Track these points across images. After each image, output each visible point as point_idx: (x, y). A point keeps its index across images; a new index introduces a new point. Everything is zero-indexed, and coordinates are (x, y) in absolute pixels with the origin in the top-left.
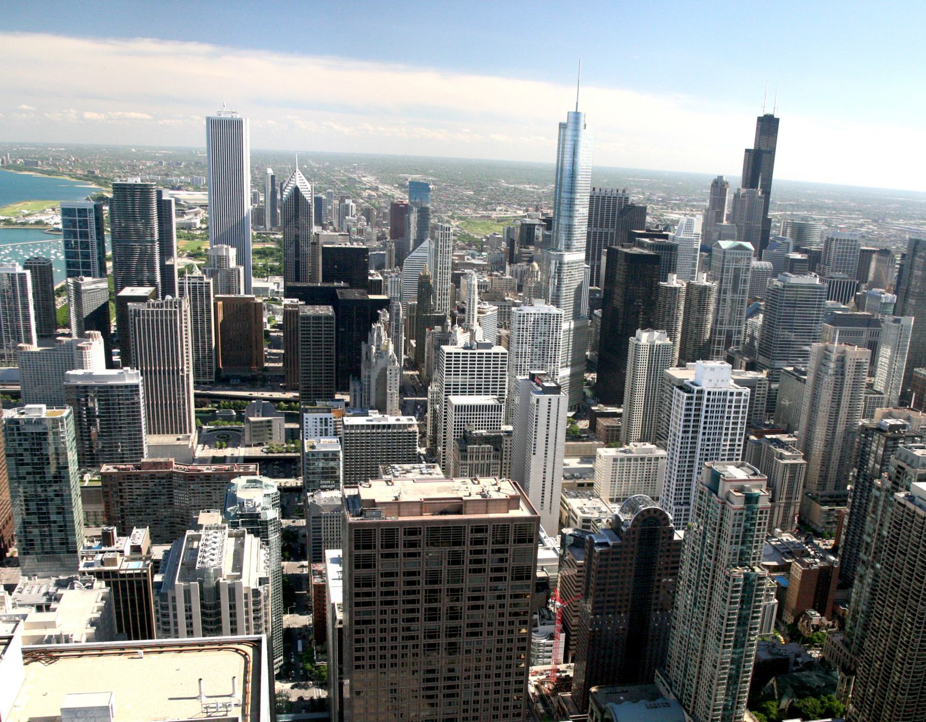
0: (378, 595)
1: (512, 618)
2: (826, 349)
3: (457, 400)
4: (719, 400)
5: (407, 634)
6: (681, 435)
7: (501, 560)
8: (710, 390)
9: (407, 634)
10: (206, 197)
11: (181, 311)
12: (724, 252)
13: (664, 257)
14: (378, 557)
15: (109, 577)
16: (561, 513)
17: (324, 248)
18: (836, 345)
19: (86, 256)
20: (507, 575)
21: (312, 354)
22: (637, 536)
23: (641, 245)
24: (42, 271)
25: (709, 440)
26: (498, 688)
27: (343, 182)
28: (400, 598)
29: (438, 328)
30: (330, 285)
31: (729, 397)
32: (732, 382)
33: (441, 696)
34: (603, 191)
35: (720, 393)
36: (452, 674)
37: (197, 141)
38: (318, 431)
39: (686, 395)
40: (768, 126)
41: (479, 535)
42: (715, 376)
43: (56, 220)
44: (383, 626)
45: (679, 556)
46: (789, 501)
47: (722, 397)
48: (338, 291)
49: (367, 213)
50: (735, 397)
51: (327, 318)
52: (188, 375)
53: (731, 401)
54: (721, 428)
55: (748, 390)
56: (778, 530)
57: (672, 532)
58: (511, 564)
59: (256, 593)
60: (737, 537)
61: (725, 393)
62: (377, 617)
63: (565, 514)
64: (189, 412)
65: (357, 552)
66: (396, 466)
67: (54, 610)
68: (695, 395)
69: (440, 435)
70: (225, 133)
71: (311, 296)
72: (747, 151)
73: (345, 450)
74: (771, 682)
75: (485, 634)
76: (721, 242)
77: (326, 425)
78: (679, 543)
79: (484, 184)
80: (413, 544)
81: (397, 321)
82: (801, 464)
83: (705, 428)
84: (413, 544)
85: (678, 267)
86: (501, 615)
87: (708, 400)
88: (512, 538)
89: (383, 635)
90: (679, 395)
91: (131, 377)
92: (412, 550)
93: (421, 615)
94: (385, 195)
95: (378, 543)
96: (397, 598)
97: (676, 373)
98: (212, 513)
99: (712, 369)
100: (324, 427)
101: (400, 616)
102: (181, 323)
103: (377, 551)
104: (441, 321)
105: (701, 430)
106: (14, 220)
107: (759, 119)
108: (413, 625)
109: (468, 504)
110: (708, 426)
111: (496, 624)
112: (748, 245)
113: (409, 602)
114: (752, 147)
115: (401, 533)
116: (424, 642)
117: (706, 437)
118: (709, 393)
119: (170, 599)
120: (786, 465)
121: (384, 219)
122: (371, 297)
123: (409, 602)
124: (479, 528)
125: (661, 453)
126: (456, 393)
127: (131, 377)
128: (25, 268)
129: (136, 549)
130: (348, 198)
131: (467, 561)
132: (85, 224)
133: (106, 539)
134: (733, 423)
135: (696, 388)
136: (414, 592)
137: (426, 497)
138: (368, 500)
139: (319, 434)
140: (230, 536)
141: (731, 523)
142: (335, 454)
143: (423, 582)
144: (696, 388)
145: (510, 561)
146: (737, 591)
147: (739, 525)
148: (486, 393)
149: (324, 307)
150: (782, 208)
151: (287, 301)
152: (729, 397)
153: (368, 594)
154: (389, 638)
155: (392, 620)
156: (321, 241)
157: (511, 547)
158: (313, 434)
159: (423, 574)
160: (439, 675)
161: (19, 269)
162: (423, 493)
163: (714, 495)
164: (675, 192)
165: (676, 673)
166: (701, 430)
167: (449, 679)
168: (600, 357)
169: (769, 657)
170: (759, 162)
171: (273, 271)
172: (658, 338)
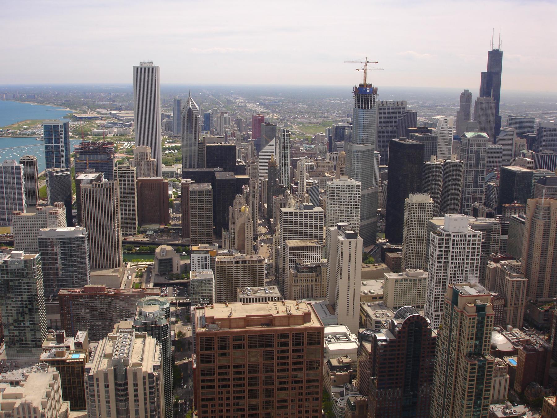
2: (537, 202)
4: (461, 241)
5: (236, 407)
6: (436, 264)
7: (299, 357)
8: (454, 234)
9: (236, 407)
10: (133, 115)
12: (469, 140)
13: (429, 144)
15: (59, 364)
16: (361, 318)
17: (207, 146)
18: (543, 200)
19: (58, 154)
20: (304, 366)
21: (197, 215)
23: (412, 138)
24: (30, 165)
25: (455, 267)
27: (224, 102)
28: (231, 383)
29: (281, 196)
30: (212, 170)
32: (469, 227)
34: (384, 103)
35: (461, 236)
37: (126, 79)
38: (201, 265)
39: (438, 237)
40: (495, 57)
41: (283, 340)
42: (456, 223)
43: (41, 131)
44: (221, 402)
45: (435, 348)
46: (516, 306)
48: (216, 173)
49: (238, 122)
50: (471, 238)
52: (118, 230)
53: (469, 241)
55: (481, 233)
56: (510, 326)
57: (430, 331)
58: (305, 359)
59: (151, 375)
61: (465, 236)
62: (217, 396)
63: (364, 318)
64: (119, 253)
66: (249, 288)
67: (22, 386)
68: (444, 237)
70: (146, 75)
71: (199, 178)
72: (482, 73)
73: (217, 279)
76: (466, 134)
77: (206, 261)
78: (434, 338)
81: (254, 192)
82: (524, 281)
83: (452, 259)
85: (438, 149)
86: (301, 394)
88: (305, 342)
89: (221, 408)
91: (79, 231)
93: (246, 394)
94: (251, 110)
95: (216, 347)
96: (233, 383)
97: (436, 221)
98: (128, 321)
99: (456, 220)
100: (204, 263)
101: (232, 395)
102: (114, 197)
103: (216, 352)
104: (283, 191)
105: (450, 261)
106: (18, 132)
108: (241, 402)
109: (276, 319)
110: (454, 258)
112: (484, 134)
113: (238, 385)
114: (486, 71)
115: (276, 337)
116: (248, 412)
118: (454, 236)
119: (95, 380)
120: (513, 281)
121: (249, 126)
122: (237, 177)
123: (238, 385)
124: (284, 335)
125: (426, 274)
126: (290, 238)
127: (79, 231)
128: (21, 163)
129: (78, 345)
130: (226, 113)
131: (276, 358)
132: (57, 135)
133: (60, 339)
135: (445, 233)
136: (241, 379)
137: (248, 314)
138: (210, 318)
139: (201, 267)
140: (137, 337)
141: (468, 325)
142: (210, 280)
143: (246, 372)
145: (305, 357)
147: (473, 327)
148: (311, 238)
149: (206, 185)
151: (183, 181)
152: (467, 238)
153: (211, 381)
154: (224, 410)
155: (227, 398)
156: (206, 142)
157: (305, 347)
158: (197, 267)
159: (246, 367)
161: (17, 164)
162: (247, 312)
163: (455, 306)
164: (436, 103)
166: (450, 261)
168: (388, 211)
169: (503, 416)
170: (491, 80)
171: (177, 161)
172: (424, 199)
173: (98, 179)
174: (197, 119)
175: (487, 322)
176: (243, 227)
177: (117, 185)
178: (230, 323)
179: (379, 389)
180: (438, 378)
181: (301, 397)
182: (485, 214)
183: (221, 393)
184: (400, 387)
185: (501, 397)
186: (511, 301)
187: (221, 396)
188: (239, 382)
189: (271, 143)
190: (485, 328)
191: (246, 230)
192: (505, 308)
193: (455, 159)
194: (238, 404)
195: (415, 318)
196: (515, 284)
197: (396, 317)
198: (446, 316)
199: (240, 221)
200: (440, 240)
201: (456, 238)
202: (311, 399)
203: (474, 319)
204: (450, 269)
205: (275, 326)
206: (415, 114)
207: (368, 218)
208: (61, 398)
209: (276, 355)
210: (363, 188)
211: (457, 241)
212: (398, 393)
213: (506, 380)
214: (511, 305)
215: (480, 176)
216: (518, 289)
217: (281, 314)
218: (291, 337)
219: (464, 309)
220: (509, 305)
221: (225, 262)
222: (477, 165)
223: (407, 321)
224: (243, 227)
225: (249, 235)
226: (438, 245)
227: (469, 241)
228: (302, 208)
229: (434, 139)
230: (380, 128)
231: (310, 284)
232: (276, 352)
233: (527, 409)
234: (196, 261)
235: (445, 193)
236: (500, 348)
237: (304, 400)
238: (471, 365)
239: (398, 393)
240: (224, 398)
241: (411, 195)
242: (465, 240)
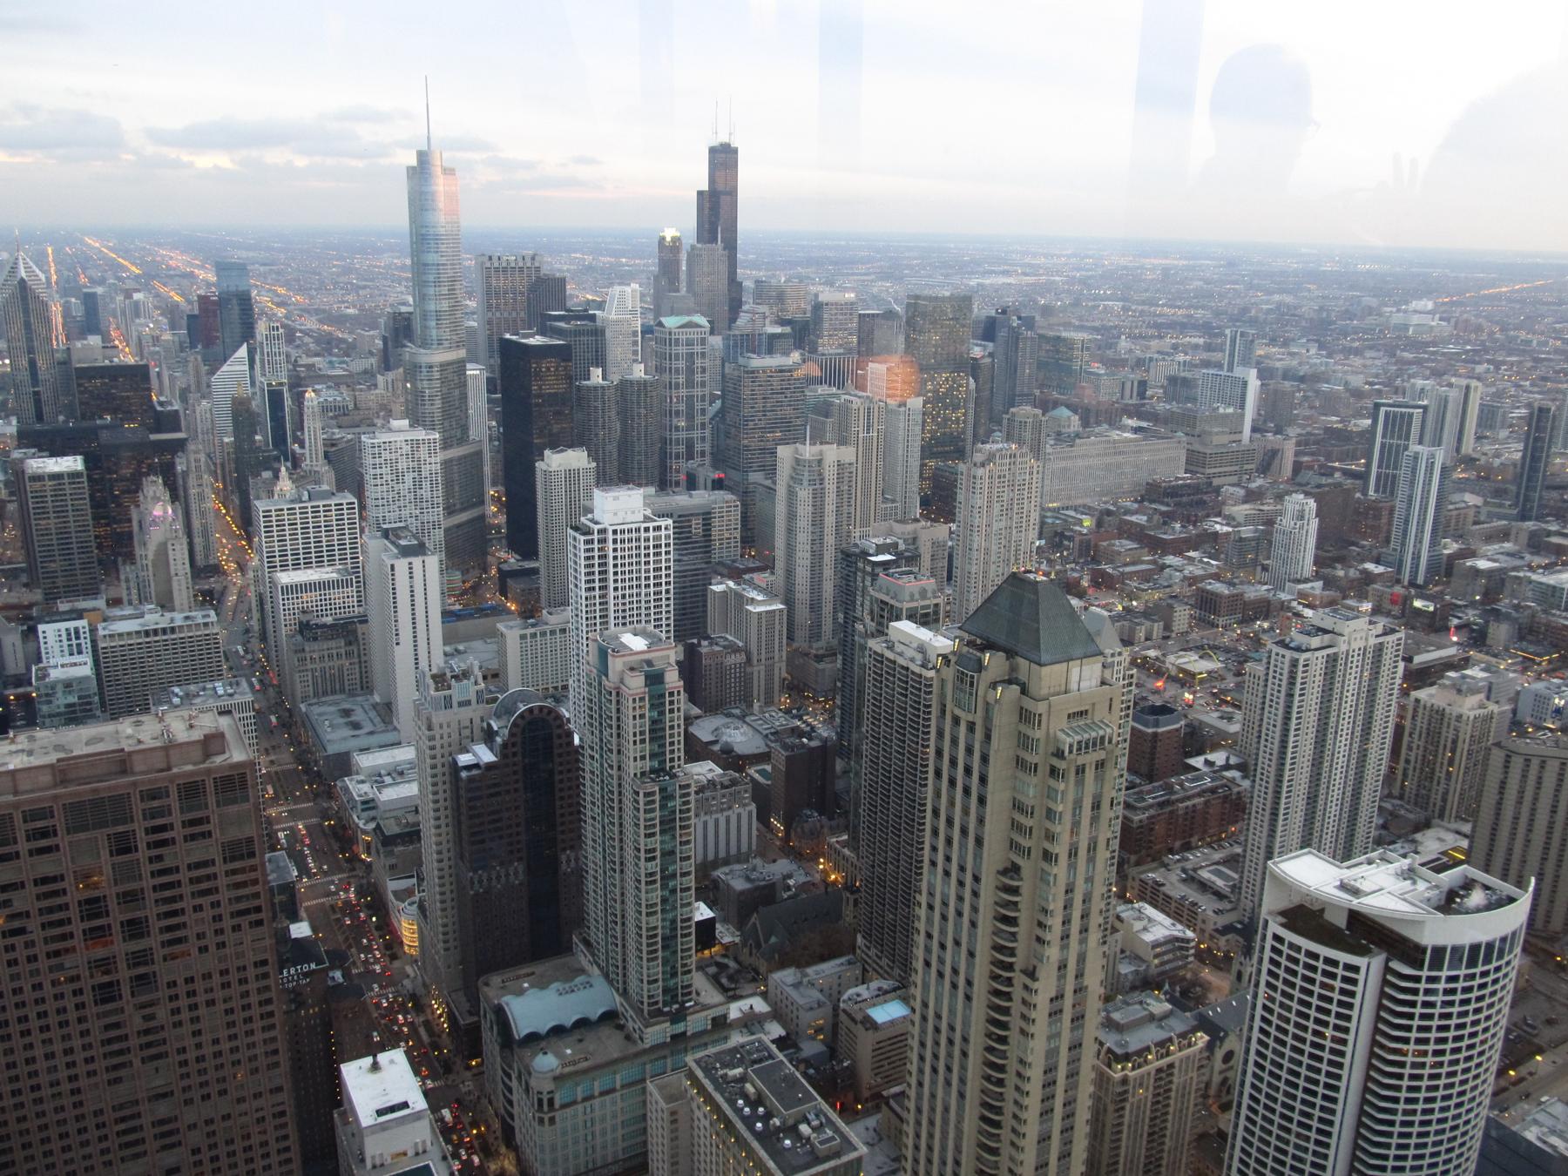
0: (185, 881)
3: (285, 578)
4: (630, 540)
22: (517, 749)
25: (624, 596)
31: (643, 535)
33: (137, 1062)
35: (630, 531)
38: (66, 648)
39: (582, 538)
40: (723, 159)
51: (74, 475)
60: (642, 733)
66: (177, 690)
68: (596, 537)
69: (270, 626)
72: (700, 193)
75: (195, 952)
80: (44, 833)
83: (616, 581)
105: (612, 585)
107: (712, 151)
108: (68, 961)
109: (135, 757)
111: (210, 934)
114: (705, 187)
117: (620, 593)
118: (615, 532)
120: (760, 614)
131: (142, 846)
135: (596, 527)
141: (631, 714)
144: (596, 527)
145: (217, 834)
146: (653, 810)
148: (320, 563)
150: (755, 265)
152: (643, 535)
156: (74, 357)
157: (213, 810)
165: (596, 935)
169: (748, 886)
170: (717, 207)
172: (575, 459)
175: (671, 703)
176: (162, 550)
178: (14, 780)
182: (709, 484)
184: (520, 859)
186: (759, 654)
189: (237, 355)
191: (171, 557)
192: (749, 670)
193: (639, 372)
195: (536, 712)
197: (498, 716)
199: (155, 536)
201: (619, 537)
202: (245, 925)
203: (642, 699)
204: (612, 602)
207: (463, 510)
209: (142, 839)
210: (446, 444)
212: (516, 873)
213: (750, 813)
216: (770, 627)
219: (622, 681)
221: (129, 634)
222: (690, 384)
224: (162, 550)
225: (180, 567)
228: (306, 497)
231: (337, 663)
234: (52, 639)
235: (625, 445)
236: (740, 749)
238: (646, 795)
239: (516, 873)
240: (22, 959)
242: (638, 540)
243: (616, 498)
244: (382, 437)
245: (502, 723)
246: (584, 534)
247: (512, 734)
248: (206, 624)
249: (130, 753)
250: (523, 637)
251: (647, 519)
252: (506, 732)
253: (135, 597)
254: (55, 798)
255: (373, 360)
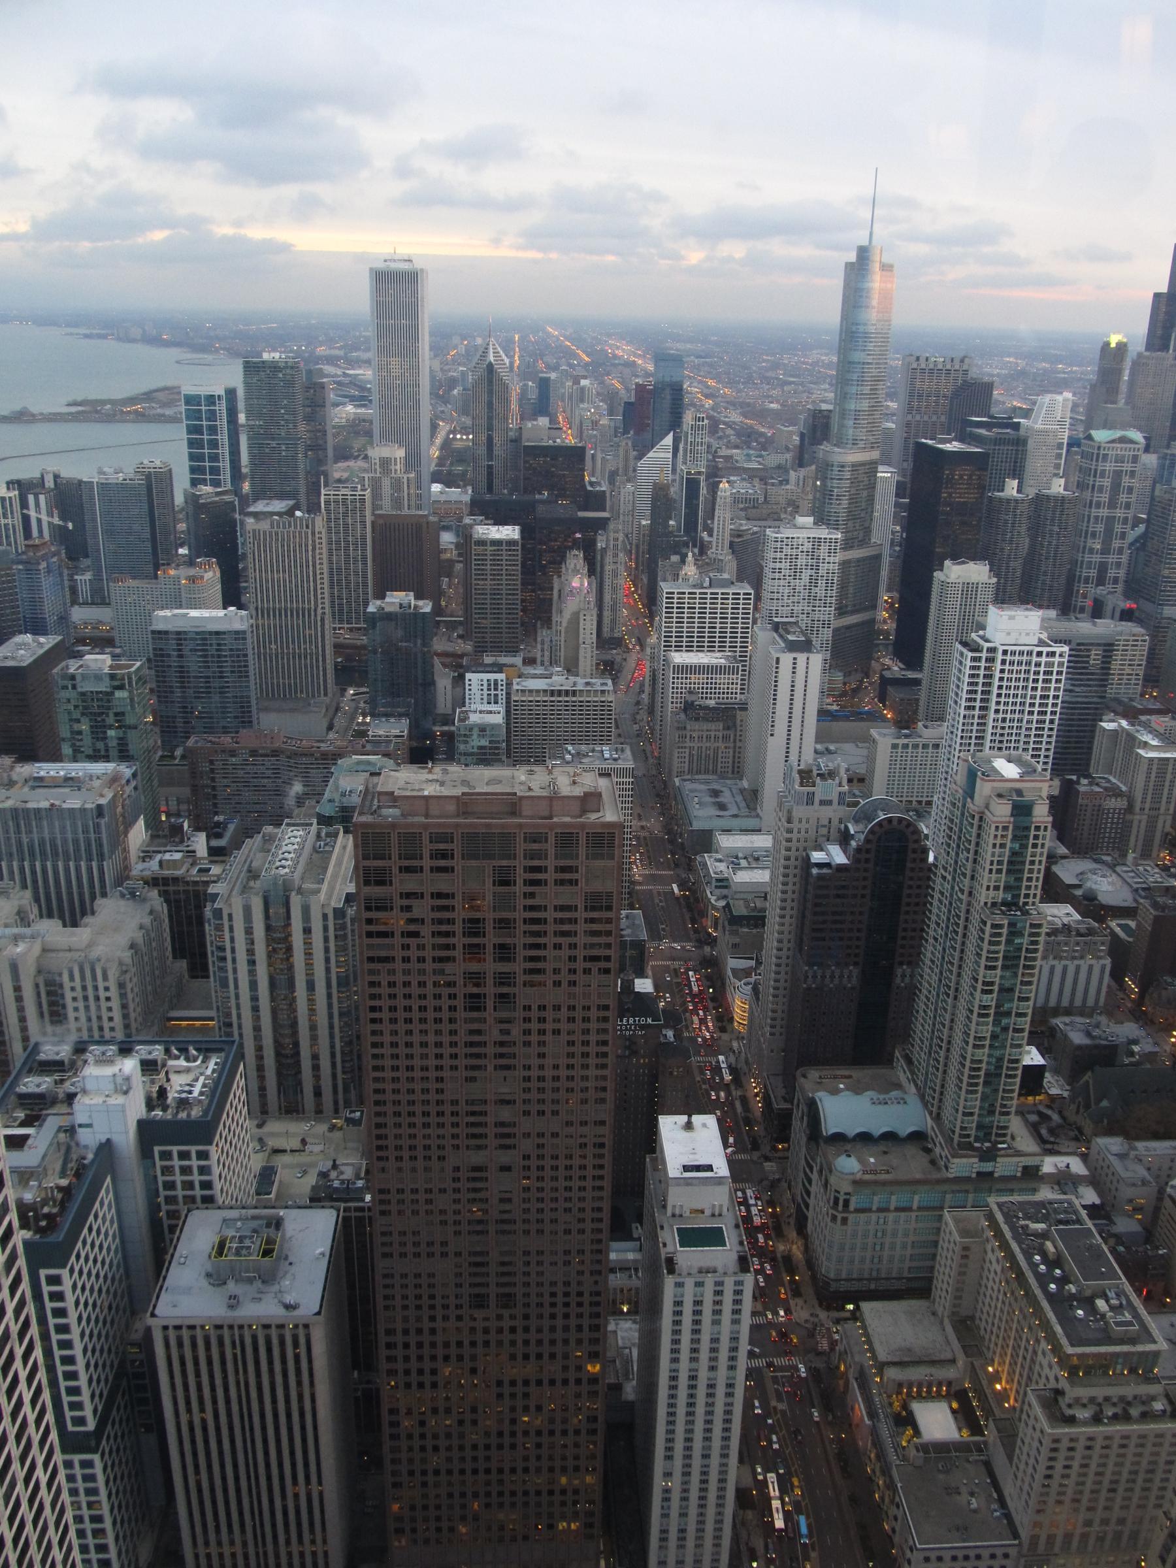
1: (588, 965)
4: (1020, 663)
11: (313, 534)
14: (395, 870)
25: (1004, 720)
26: (571, 1061)
35: (1021, 653)
36: (505, 1038)
37: (359, 301)
39: (970, 654)
41: (536, 846)
47: (1025, 658)
51: (511, 543)
53: (1038, 665)
54: (1023, 704)
60: (1000, 863)
62: (399, 954)
65: (367, 863)
66: (570, 748)
68: (984, 655)
74: (1086, 1078)
79: (747, 356)
83: (998, 703)
84: (444, 855)
87: (1003, 662)
90: (962, 654)
92: (442, 863)
105: (993, 707)
108: (449, 967)
109: (524, 802)
111: (565, 972)
114: (1164, 289)
115: (520, 839)
117: (1000, 716)
118: (1005, 652)
119: (225, 917)
120: (1151, 760)
122: (581, 514)
126: (679, 648)
131: (519, 882)
132: (212, 415)
134: (1042, 697)
135: (986, 645)
138: (387, 793)
144: (986, 645)
145: (582, 884)
148: (711, 649)
152: (1035, 659)
156: (524, 437)
160: (487, 1038)
167: (502, 1044)
169: (1087, 1041)
172: (977, 572)
173: (290, 512)
174: (506, 387)
176: (575, 619)
177: (320, 523)
179: (811, 965)
180: (930, 951)
181: (572, 965)
182: (1117, 614)
183: (406, 947)
184: (856, 964)
185: (1091, 1002)
187: (406, 953)
188: (444, 928)
190: (1030, 850)
192: (1129, 817)
193: (1058, 487)
194: (442, 972)
195: (895, 823)
196: (1155, 767)
197: (856, 820)
198: (952, 821)
199: (571, 606)
200: (974, 659)
201: (1008, 658)
202: (595, 971)
205: (521, 816)
206: (988, 388)
207: (853, 612)
208: (169, 953)
210: (847, 545)
211: (1012, 663)
214: (1142, 809)
215: (1118, 528)
216: (1161, 774)
217: (537, 792)
218: (552, 839)
219: (987, 807)
220: (1137, 809)
223: (877, 829)
224: (575, 619)
226: (968, 672)
227: (1038, 665)
228: (707, 584)
229: (1020, 443)
230: (909, 417)
232: (520, 871)
233: (1143, 1033)
234: (475, 687)
235: (1032, 562)
236: (1104, 899)
237: (580, 972)
238: (994, 926)
240: (414, 959)
241: (947, 563)
242: (1029, 663)
243: (1011, 618)
244: (787, 532)
245: (860, 827)
246: (972, 651)
247: (867, 841)
248: (603, 692)
249: (522, 798)
250: (895, 746)
251: (1041, 643)
252: (862, 837)
253: (546, 659)
254: (457, 825)
255: (788, 456)
